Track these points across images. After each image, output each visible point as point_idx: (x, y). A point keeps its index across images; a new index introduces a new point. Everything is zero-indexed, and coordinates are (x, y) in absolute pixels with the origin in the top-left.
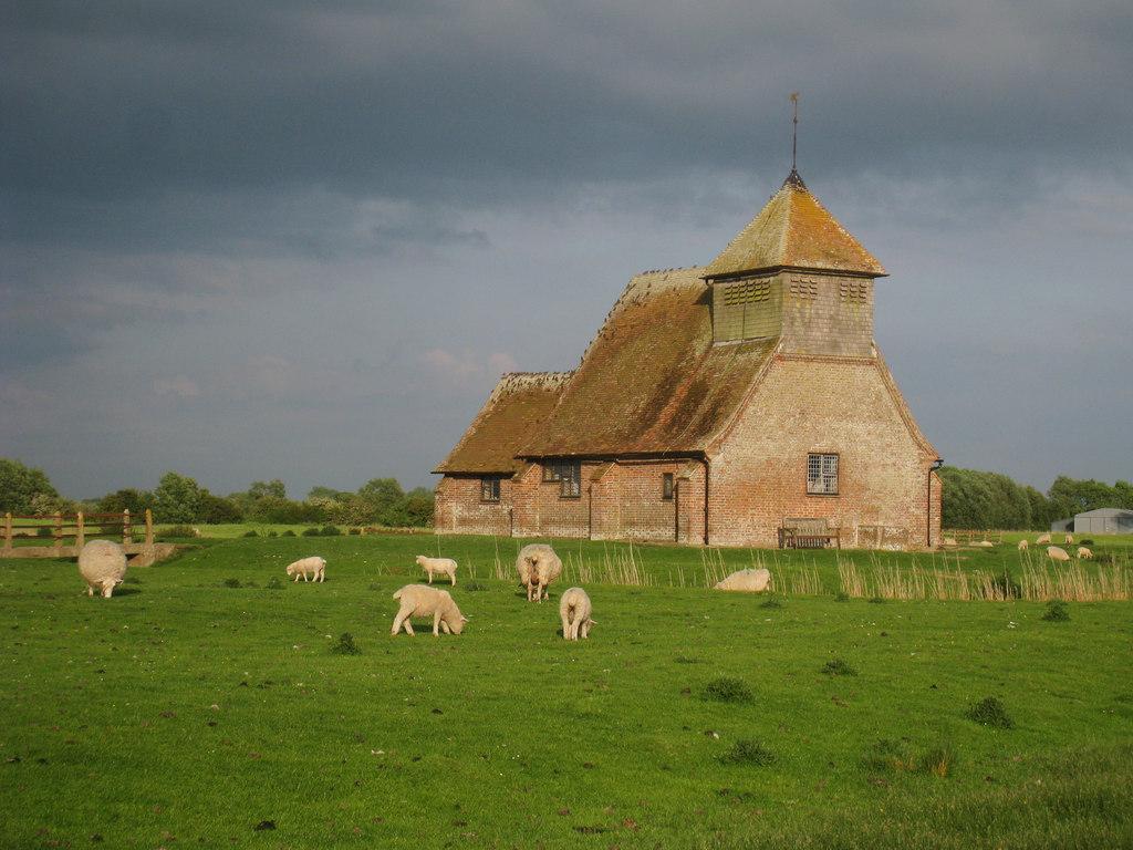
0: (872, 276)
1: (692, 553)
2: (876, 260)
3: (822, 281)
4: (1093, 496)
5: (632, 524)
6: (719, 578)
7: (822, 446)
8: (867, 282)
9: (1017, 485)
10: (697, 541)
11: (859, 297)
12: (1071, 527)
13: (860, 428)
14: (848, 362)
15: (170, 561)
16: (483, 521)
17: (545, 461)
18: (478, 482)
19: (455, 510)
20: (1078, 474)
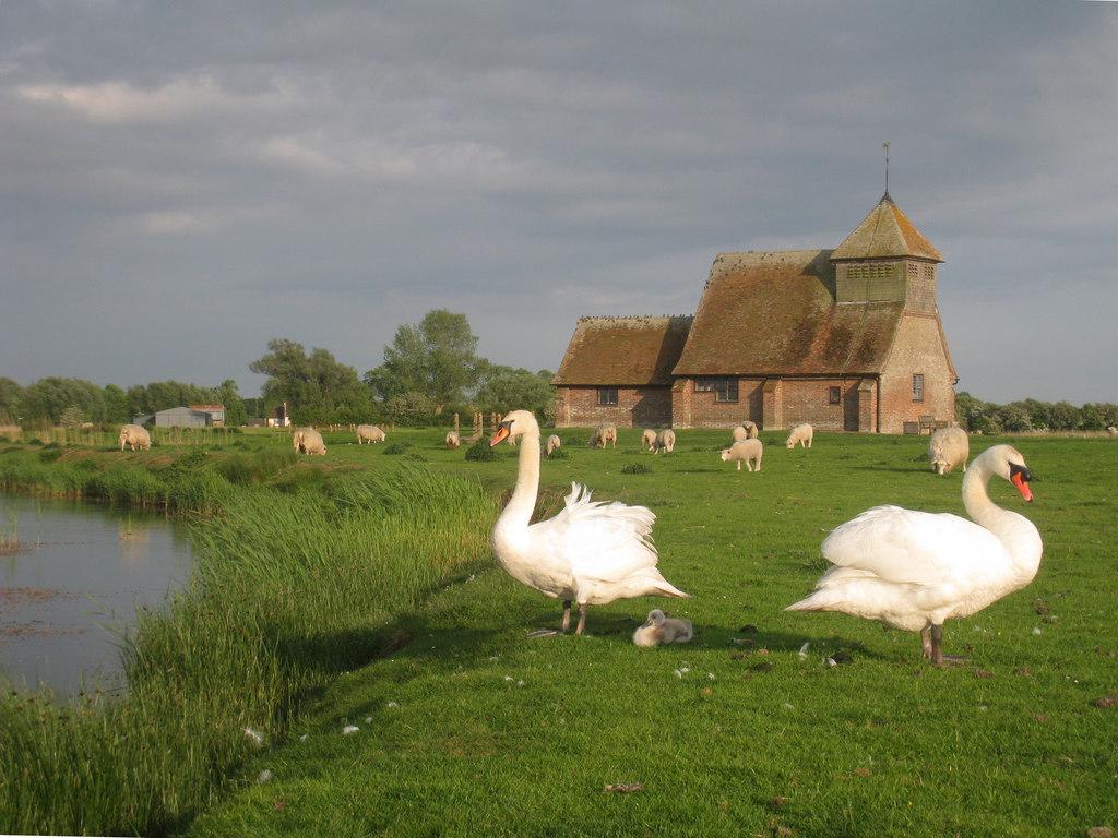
0: (936, 262)
3: (919, 265)
7: (916, 371)
8: (934, 266)
10: (874, 431)
11: (930, 274)
13: (930, 358)
14: (927, 317)
18: (595, 391)
20: (162, 378)
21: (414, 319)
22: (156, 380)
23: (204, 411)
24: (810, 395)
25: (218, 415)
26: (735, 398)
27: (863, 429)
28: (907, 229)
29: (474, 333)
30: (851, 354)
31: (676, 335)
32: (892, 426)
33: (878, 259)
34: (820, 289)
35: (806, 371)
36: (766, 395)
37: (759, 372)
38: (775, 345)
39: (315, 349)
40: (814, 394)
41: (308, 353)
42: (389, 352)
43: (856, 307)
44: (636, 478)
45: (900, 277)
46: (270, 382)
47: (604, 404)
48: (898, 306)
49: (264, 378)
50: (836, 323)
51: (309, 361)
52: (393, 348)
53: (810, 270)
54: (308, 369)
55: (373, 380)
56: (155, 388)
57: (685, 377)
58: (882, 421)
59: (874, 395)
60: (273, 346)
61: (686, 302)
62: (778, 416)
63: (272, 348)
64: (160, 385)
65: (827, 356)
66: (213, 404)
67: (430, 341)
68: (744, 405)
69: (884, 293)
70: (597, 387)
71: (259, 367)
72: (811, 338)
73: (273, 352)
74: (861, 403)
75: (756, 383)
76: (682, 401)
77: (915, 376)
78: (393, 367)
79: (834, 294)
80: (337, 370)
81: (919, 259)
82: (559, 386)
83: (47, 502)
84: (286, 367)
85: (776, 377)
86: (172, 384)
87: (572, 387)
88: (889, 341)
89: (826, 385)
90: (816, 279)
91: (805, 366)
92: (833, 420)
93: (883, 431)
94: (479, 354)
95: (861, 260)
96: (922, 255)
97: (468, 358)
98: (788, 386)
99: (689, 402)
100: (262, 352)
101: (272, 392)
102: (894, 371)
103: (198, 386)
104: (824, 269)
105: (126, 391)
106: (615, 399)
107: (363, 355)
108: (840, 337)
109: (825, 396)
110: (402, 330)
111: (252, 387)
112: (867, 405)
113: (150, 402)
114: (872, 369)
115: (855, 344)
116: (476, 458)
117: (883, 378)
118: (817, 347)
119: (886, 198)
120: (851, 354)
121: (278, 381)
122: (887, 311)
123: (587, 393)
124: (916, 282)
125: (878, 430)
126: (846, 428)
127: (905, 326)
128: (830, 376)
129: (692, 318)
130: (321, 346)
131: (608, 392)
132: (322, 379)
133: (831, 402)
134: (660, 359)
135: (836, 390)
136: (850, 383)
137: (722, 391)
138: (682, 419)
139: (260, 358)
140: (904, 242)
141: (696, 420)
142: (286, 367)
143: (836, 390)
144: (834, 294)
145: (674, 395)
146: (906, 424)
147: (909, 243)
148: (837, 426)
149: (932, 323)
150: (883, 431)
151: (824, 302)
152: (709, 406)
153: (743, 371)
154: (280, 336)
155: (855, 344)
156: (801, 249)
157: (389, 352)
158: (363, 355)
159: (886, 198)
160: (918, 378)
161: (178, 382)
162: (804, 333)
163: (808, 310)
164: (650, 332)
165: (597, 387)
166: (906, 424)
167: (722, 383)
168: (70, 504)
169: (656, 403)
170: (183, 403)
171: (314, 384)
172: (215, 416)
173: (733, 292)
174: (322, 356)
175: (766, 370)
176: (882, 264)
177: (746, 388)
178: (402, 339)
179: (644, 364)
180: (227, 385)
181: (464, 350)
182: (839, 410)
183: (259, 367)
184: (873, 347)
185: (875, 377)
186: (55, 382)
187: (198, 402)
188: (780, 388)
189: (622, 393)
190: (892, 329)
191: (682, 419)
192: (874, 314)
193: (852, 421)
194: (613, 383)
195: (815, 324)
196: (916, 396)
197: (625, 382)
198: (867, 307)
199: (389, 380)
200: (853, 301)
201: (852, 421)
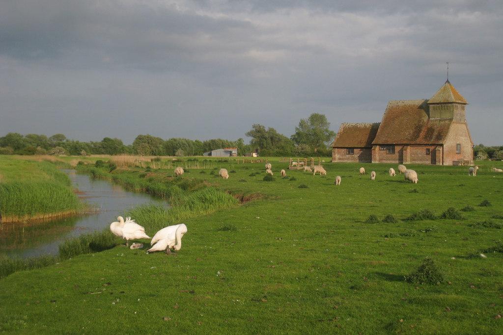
0: (465, 104)
1: (441, 166)
2: (466, 100)
3: (459, 105)
4: (222, 145)
5: (414, 160)
6: (466, 173)
7: (458, 143)
8: (465, 106)
9: (216, 139)
10: (441, 164)
11: (463, 109)
12: (210, 154)
13: (463, 138)
14: (462, 123)
15: (416, 167)
16: (348, 159)
17: (380, 145)
18: (346, 149)
19: (337, 156)
20: (215, 137)
21: (306, 117)
22: (213, 138)
23: (230, 150)
24: (419, 151)
25: (234, 152)
26: (394, 152)
27: (438, 164)
28: (454, 92)
29: (328, 121)
30: (434, 137)
31: (374, 129)
32: (448, 162)
33: (446, 103)
34: (424, 114)
35: (418, 143)
36: (404, 151)
37: (402, 143)
38: (408, 133)
39: (269, 128)
40: (421, 151)
41: (267, 129)
42: (297, 129)
43: (436, 120)
44: (303, 190)
45: (452, 110)
46: (253, 140)
47: (349, 154)
48: (451, 120)
49: (251, 138)
50: (429, 126)
51: (267, 132)
52: (298, 128)
53: (421, 107)
54: (267, 135)
55: (294, 139)
56: (213, 141)
57: (376, 145)
58: (444, 160)
59: (441, 151)
60: (254, 127)
61: (377, 117)
62: (408, 159)
63: (253, 128)
64: (215, 140)
65: (426, 137)
66: (233, 147)
67: (312, 125)
68: (397, 155)
69: (447, 116)
70: (347, 148)
71: (249, 134)
72: (420, 131)
73: (254, 129)
74: (437, 154)
75: (401, 147)
76: (375, 153)
77: (457, 145)
78: (298, 134)
79: (429, 115)
80: (277, 135)
81: (459, 103)
82: (334, 148)
83: (134, 192)
84: (259, 134)
85: (407, 145)
86: (220, 140)
87: (338, 148)
88: (447, 133)
89: (425, 148)
90: (422, 110)
91: (418, 141)
92: (427, 160)
93: (445, 164)
94: (330, 129)
95: (438, 104)
96: (460, 102)
97: (327, 131)
98: (412, 148)
99: (378, 154)
100: (250, 129)
101: (253, 144)
102: (449, 143)
103: (229, 141)
104: (425, 107)
105: (203, 142)
106: (353, 152)
107: (287, 131)
108: (430, 131)
109: (424, 152)
110: (301, 121)
111: (247, 141)
112: (439, 155)
113: (212, 146)
114: (441, 142)
115: (436, 133)
116: (267, 180)
117: (444, 146)
118: (422, 134)
119: (448, 81)
120: (434, 137)
121: (255, 139)
122: (447, 122)
123: (343, 150)
124: (457, 111)
125: (443, 164)
126: (431, 163)
127: (454, 127)
128: (426, 145)
129: (380, 123)
130: (271, 127)
131: (351, 150)
132: (272, 139)
133: (427, 154)
134: (369, 138)
135: (428, 150)
136: (433, 147)
137: (389, 150)
138: (375, 160)
139: (249, 131)
140: (453, 98)
141: (380, 160)
142: (259, 134)
143: (428, 150)
144: (429, 115)
145: (373, 151)
146: (453, 162)
147: (455, 98)
148: (429, 162)
149: (464, 126)
150: (445, 164)
151: (425, 119)
152: (385, 155)
153: (397, 143)
154: (257, 123)
155: (436, 133)
156: (418, 100)
157: (297, 129)
158: (287, 131)
159: (448, 81)
160: (458, 145)
161: (221, 139)
162: (418, 129)
163: (419, 121)
164: (365, 128)
165: (347, 148)
166: (453, 162)
167: (389, 147)
168: (142, 192)
169: (366, 154)
170: (223, 147)
171: (269, 141)
172: (233, 152)
173: (394, 115)
174: (272, 130)
175: (404, 142)
176: (445, 105)
177: (398, 149)
178: (302, 124)
179: (363, 139)
180: (240, 140)
181: (325, 128)
182: (430, 157)
183: (249, 134)
184: (441, 134)
185: (442, 145)
186: (175, 140)
187: (229, 147)
188: (409, 150)
189: (355, 150)
190: (448, 128)
191: (375, 160)
192: (442, 123)
193: (434, 160)
194: (352, 146)
195: (422, 126)
196: (458, 152)
197: (356, 146)
198: (440, 120)
199: (298, 137)
200: (435, 118)
201: (434, 160)
